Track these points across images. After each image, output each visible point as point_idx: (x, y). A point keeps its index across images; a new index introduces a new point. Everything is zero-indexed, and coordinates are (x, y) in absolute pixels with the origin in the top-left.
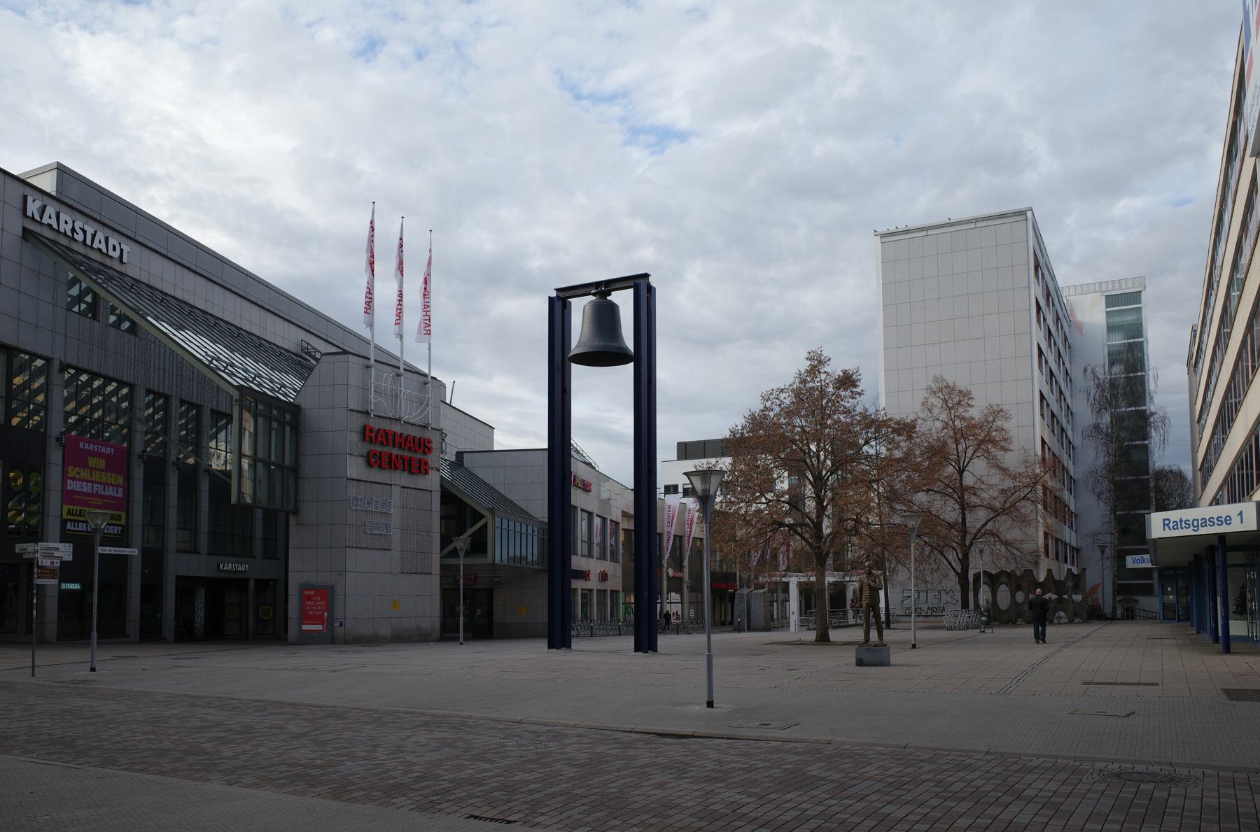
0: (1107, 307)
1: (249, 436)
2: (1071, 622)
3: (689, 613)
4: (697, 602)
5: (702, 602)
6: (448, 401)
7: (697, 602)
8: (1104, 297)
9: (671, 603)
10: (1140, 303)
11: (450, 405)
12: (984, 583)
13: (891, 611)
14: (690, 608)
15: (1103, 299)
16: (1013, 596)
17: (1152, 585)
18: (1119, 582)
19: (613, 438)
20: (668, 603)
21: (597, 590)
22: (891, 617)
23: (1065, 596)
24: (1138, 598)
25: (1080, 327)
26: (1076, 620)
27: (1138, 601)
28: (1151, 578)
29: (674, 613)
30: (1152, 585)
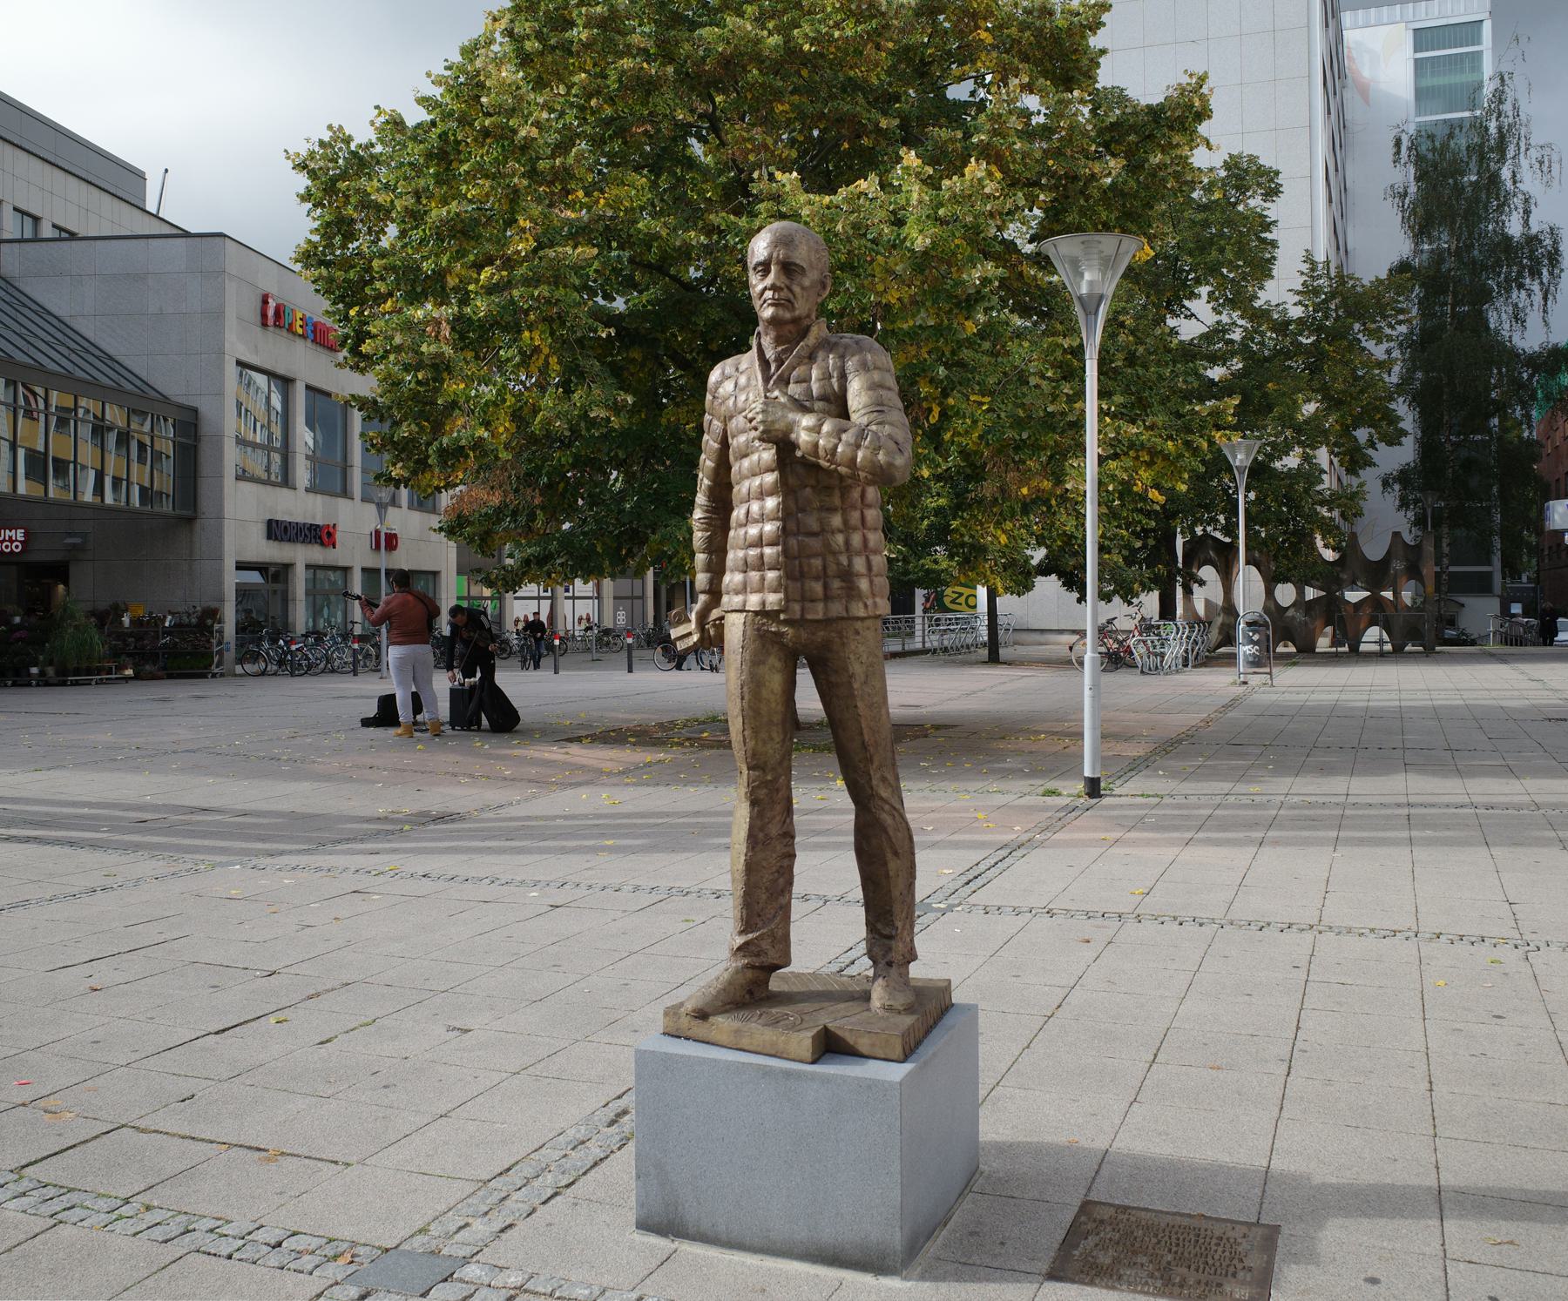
0: (1415, 51)
1: (1249, 782)
2: (1398, 653)
3: (615, 617)
4: (632, 598)
5: (643, 597)
6: (151, 206)
7: (632, 598)
8: (1411, 32)
9: (574, 598)
10: (1479, 43)
11: (156, 216)
12: (1248, 563)
13: (1001, 620)
14: (616, 610)
15: (1410, 36)
16: (1270, 593)
17: (1489, 575)
18: (1452, 569)
19: (842, 811)
20: (566, 598)
21: (364, 570)
22: (1001, 633)
23: (1388, 595)
24: (1462, 600)
25: (1364, 91)
26: (1409, 648)
27: (1463, 605)
28: (1489, 563)
29: (580, 619)
30: (1489, 575)
